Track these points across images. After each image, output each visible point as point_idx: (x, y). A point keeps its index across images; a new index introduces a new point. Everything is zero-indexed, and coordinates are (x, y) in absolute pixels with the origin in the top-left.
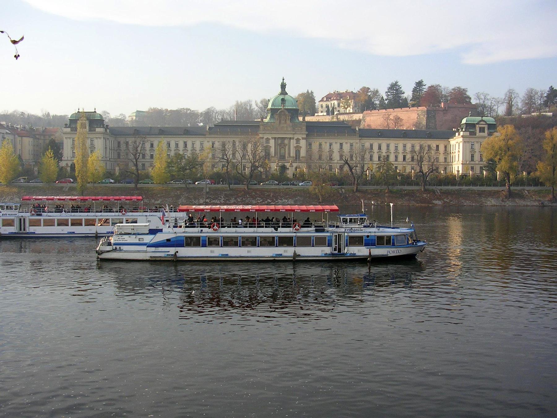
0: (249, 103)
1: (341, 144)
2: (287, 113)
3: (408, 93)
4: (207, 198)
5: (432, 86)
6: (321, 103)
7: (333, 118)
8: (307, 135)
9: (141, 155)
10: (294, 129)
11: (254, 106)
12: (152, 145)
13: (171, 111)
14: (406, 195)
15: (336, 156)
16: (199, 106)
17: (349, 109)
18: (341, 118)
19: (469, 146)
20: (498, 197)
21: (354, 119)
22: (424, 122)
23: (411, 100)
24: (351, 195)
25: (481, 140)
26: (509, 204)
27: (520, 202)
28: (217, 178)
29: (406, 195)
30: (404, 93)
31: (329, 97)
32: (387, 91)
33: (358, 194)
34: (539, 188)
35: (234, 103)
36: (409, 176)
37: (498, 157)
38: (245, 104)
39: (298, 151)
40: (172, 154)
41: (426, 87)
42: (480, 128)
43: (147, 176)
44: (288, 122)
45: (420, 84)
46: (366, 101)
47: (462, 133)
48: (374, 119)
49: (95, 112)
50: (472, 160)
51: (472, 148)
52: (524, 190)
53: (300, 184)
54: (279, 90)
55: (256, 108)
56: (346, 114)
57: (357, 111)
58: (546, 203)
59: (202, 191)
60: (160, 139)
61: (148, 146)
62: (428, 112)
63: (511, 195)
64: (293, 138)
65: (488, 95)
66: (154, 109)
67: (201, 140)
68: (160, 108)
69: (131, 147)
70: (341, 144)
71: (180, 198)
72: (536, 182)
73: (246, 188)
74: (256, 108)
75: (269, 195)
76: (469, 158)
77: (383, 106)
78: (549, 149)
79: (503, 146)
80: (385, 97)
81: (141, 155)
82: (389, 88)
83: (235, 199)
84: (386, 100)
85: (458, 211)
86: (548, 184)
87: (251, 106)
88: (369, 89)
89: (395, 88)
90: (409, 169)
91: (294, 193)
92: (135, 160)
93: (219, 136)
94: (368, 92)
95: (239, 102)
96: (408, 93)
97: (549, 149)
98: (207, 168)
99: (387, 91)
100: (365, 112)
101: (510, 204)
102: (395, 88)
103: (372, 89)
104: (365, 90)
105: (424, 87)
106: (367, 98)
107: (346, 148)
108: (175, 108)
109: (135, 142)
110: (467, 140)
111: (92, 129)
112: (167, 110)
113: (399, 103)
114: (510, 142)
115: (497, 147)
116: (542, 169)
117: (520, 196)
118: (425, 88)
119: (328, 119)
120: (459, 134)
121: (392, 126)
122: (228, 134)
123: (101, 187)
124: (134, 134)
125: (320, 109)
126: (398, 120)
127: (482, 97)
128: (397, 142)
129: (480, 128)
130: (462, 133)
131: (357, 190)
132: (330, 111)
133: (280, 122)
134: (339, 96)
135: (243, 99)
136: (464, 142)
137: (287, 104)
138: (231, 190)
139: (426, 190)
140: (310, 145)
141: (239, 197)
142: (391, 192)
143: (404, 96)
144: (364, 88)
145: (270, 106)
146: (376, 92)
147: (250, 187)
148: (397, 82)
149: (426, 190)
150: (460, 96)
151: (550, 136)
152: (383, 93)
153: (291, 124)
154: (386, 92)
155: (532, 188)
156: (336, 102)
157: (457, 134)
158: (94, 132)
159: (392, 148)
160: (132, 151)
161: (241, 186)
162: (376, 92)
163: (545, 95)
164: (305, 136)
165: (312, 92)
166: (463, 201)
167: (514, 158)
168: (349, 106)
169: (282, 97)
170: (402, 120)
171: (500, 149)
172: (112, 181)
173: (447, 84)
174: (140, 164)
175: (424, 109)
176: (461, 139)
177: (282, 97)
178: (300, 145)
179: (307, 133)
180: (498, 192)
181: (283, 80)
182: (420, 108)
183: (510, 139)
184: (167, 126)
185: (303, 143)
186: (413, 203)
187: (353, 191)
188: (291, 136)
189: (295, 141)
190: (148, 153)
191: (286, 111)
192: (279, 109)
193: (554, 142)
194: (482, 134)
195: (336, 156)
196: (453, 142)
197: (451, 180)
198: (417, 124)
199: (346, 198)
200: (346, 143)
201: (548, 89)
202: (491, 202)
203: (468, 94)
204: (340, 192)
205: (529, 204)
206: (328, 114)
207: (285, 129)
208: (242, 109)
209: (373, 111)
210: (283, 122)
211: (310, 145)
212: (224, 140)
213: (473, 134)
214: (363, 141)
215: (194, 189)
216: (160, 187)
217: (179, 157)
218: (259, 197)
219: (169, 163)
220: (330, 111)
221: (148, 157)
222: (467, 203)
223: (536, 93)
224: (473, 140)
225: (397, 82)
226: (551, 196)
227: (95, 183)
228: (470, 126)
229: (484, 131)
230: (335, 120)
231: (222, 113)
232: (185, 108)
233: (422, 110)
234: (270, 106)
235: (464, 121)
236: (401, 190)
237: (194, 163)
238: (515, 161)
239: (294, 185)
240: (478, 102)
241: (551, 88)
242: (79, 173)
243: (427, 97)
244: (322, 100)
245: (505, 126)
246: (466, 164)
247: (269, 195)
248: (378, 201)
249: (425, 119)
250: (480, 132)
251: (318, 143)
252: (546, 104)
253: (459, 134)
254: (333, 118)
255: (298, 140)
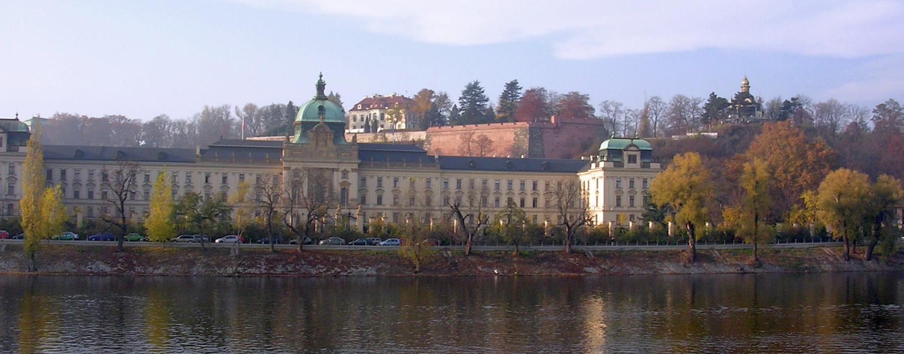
0: (225, 109)
1: (429, 182)
2: (328, 130)
3: (493, 98)
4: (239, 265)
5: (533, 91)
6: (354, 113)
7: (376, 138)
8: (359, 165)
9: (129, 194)
10: (339, 155)
11: (233, 115)
12: (147, 177)
13: (93, 120)
14: (545, 259)
15: (437, 199)
16: (141, 112)
17: (399, 123)
18: (390, 137)
19: (613, 183)
20: (678, 261)
21: (411, 139)
22: (526, 146)
23: (499, 112)
24: (462, 260)
25: (632, 175)
26: (694, 270)
27: (708, 268)
28: (251, 234)
29: (545, 259)
30: (487, 100)
31: (366, 104)
32: (461, 96)
33: (472, 259)
34: (733, 246)
35: (200, 110)
36: (541, 230)
37: (679, 201)
38: (219, 111)
39: (344, 191)
40: (181, 192)
41: (523, 91)
42: (630, 156)
43: (143, 232)
44: (330, 144)
45: (512, 86)
46: (427, 111)
47: (602, 164)
48: (447, 141)
49: (17, 119)
50: (618, 205)
51: (617, 187)
52: (712, 249)
53: (382, 243)
54: (314, 93)
55: (237, 119)
56: (396, 131)
57: (412, 127)
58: (747, 269)
59: (229, 253)
60: (161, 169)
61: (140, 179)
62: (532, 131)
63: (696, 257)
64: (337, 170)
65: (621, 105)
66: (64, 115)
67: (189, 169)
68: (73, 114)
69: (112, 180)
70: (429, 182)
71: (195, 264)
72: (729, 237)
73: (298, 249)
74: (237, 119)
75: (336, 261)
76: (614, 201)
77: (457, 120)
78: (749, 188)
79: (685, 184)
80: (459, 106)
81: (129, 194)
82: (465, 93)
83: (284, 266)
84: (461, 110)
85: (603, 287)
86: (747, 240)
87: (228, 114)
88: (432, 92)
89: (473, 92)
90: (547, 221)
91: (374, 257)
92: (119, 202)
93: (216, 165)
94: (431, 97)
95: (210, 107)
96: (493, 98)
97: (749, 188)
98: (237, 219)
99: (461, 96)
100: (430, 129)
101: (697, 271)
102: (473, 92)
103: (437, 93)
104: (426, 94)
105: (519, 91)
106: (430, 107)
107: (404, 185)
108: (99, 116)
109: (119, 173)
110: (610, 174)
111: (13, 148)
112: (85, 118)
113: (481, 115)
114: (695, 178)
115: (676, 185)
116: (731, 218)
117: (710, 259)
118: (521, 93)
119: (366, 138)
120: (597, 166)
121: (476, 153)
122: (231, 162)
123: (60, 246)
124: (118, 159)
125: (352, 122)
126: (485, 142)
127: (612, 108)
128: (498, 177)
129: (630, 156)
130: (602, 164)
131: (470, 253)
132: (370, 127)
133: (317, 144)
134: (383, 103)
135: (215, 103)
136: (606, 178)
137: (327, 114)
138: (275, 252)
139: (572, 252)
140: (363, 180)
141: (288, 263)
142: (521, 255)
143: (487, 105)
144: (425, 91)
145: (299, 118)
146: (443, 98)
147: (306, 247)
148: (477, 83)
149: (572, 252)
150: (576, 106)
151: (750, 168)
152: (455, 99)
153: (334, 147)
154: (460, 98)
155: (724, 247)
156: (378, 112)
157: (593, 165)
158: (15, 153)
159: (529, 187)
160: (114, 188)
161: (289, 246)
162: (443, 98)
163: (701, 105)
164: (356, 166)
165: (338, 96)
166: (628, 267)
167: (701, 202)
168: (399, 119)
169: (319, 103)
170: (490, 142)
171: (682, 189)
172: (76, 236)
173: (558, 87)
174: (126, 208)
175: (525, 125)
176: (601, 173)
177: (319, 103)
178: (349, 181)
179: (359, 161)
180: (676, 254)
181: (321, 76)
182: (519, 124)
183: (694, 173)
184: (92, 144)
185: (353, 178)
186: (556, 272)
187: (464, 253)
188: (334, 166)
189: (340, 174)
190: (140, 189)
191: (326, 126)
192: (315, 123)
193: (757, 178)
194: (632, 165)
195: (437, 199)
196: (583, 177)
197: (600, 237)
198: (515, 149)
199: (455, 265)
200: (404, 177)
201: (708, 97)
202: (669, 268)
203: (589, 103)
204: (445, 255)
205: (722, 270)
206: (367, 131)
207: (325, 155)
208: (215, 121)
209: (443, 128)
210: (321, 143)
211: (363, 180)
212: (260, 171)
213: (618, 165)
214: (446, 175)
215: (215, 250)
216: (161, 246)
217: (193, 198)
218: (321, 263)
219: (176, 207)
220: (370, 127)
221: (140, 197)
222: (635, 271)
223: (687, 103)
224: (619, 174)
225: (477, 83)
226: (753, 258)
227: (50, 238)
228: (614, 153)
229: (635, 162)
230: (379, 140)
231: (181, 124)
232: (117, 115)
233: (521, 128)
234: (299, 118)
235: (604, 145)
236: (536, 253)
237: (218, 208)
238: (702, 207)
239: (370, 243)
240: (606, 115)
241: (713, 96)
242: (28, 222)
243: (523, 106)
244: (355, 109)
245: (686, 155)
246: (610, 211)
247: (336, 261)
248: (503, 269)
249: (527, 140)
250: (629, 162)
251: (375, 179)
252: (705, 120)
253: (597, 166)
254: (376, 138)
255: (345, 173)
